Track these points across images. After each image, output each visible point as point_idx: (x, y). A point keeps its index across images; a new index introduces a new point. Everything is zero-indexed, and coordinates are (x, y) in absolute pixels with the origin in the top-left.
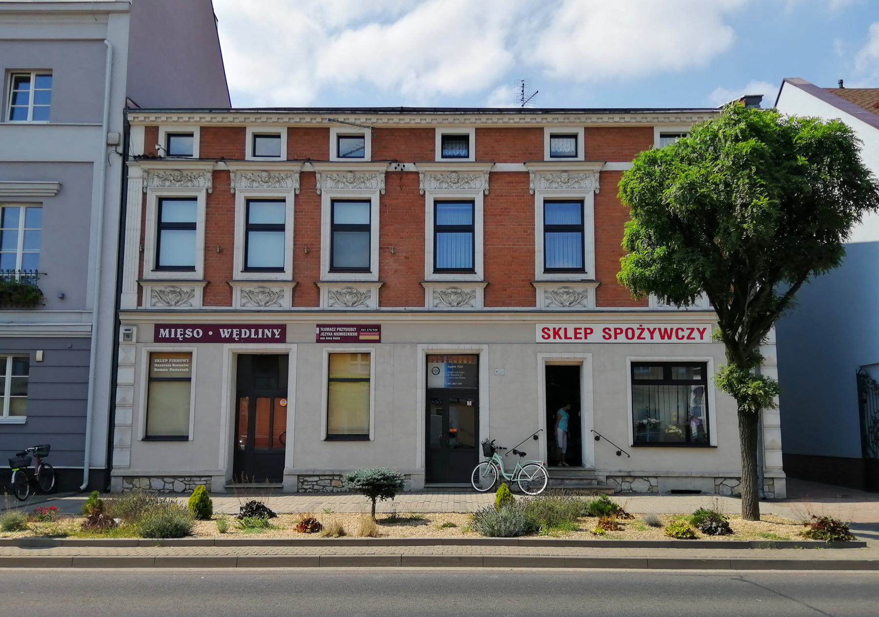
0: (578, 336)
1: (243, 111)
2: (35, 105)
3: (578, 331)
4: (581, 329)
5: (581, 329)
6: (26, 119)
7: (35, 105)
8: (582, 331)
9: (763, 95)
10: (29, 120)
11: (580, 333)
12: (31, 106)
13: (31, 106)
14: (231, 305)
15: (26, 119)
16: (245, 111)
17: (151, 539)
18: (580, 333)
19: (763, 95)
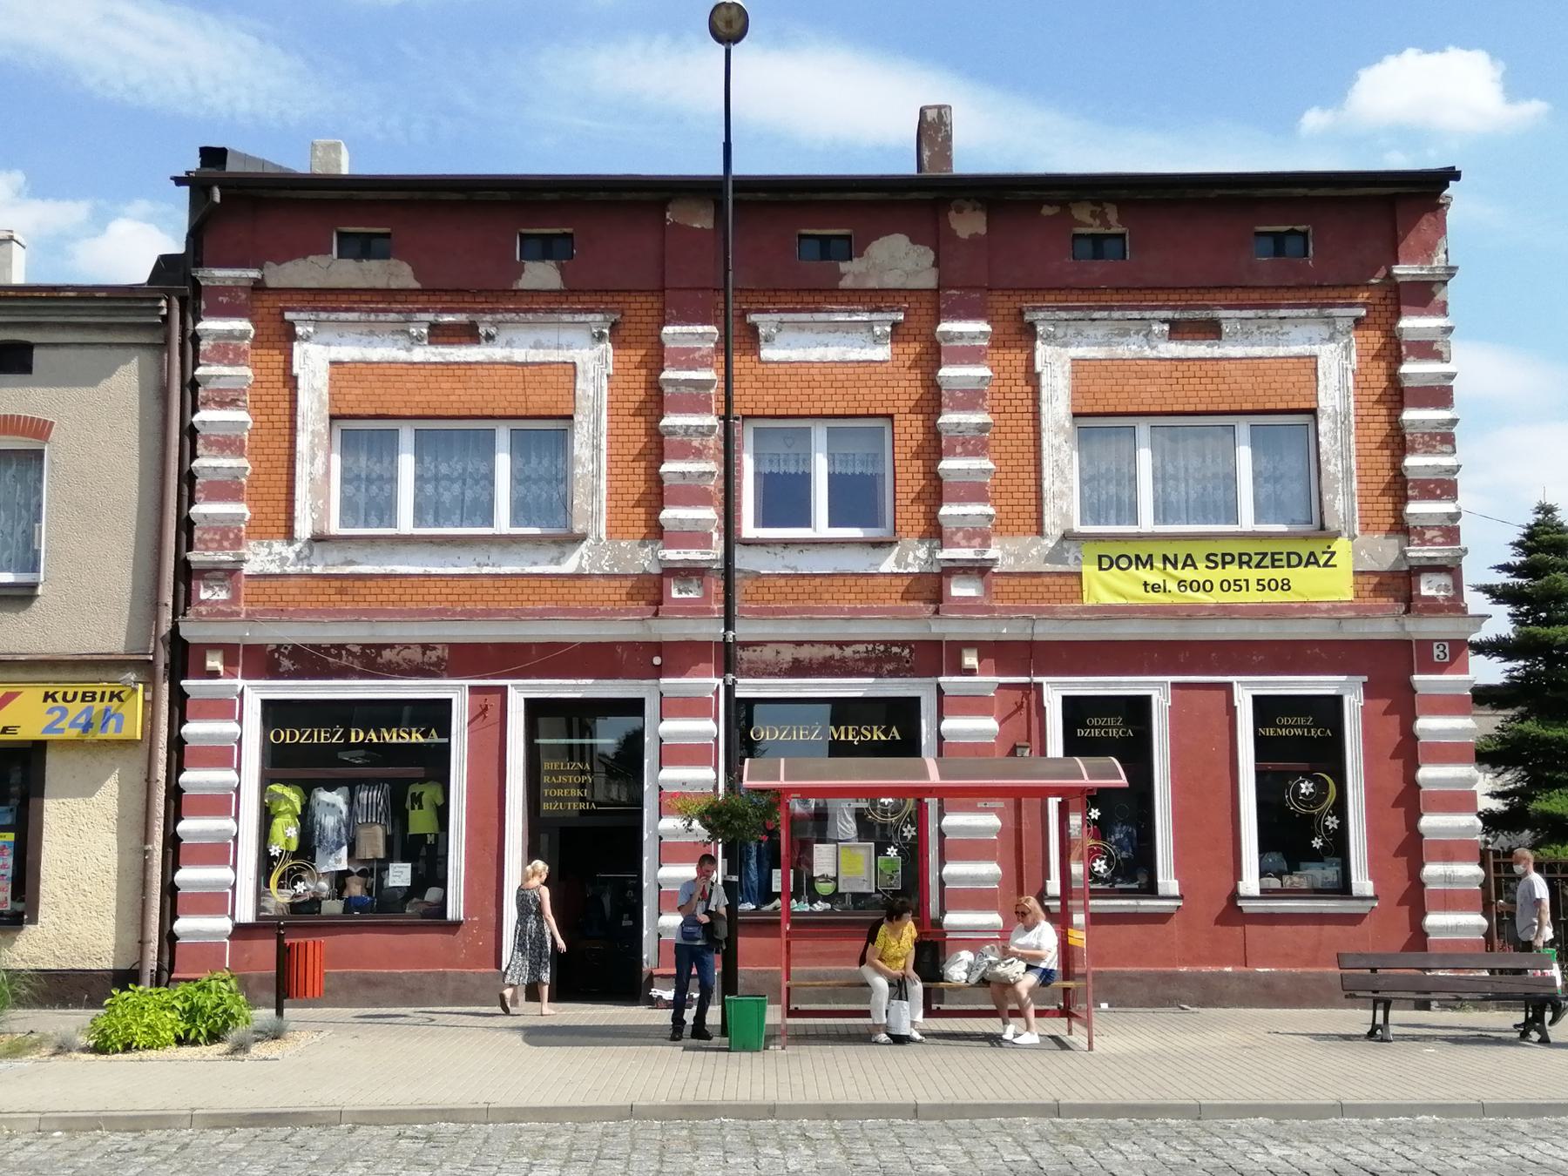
0: (1277, 563)
1: (815, 197)
2: (241, 647)
3: (1276, 557)
4: (1282, 553)
5: (1282, 553)
6: (805, 520)
7: (241, 647)
8: (1284, 557)
9: (1452, 174)
10: (821, 527)
11: (1281, 560)
12: (576, 741)
13: (576, 741)
14: (492, 525)
15: (805, 520)
16: (850, 196)
17: (1102, 969)
18: (1281, 560)
19: (1452, 174)
